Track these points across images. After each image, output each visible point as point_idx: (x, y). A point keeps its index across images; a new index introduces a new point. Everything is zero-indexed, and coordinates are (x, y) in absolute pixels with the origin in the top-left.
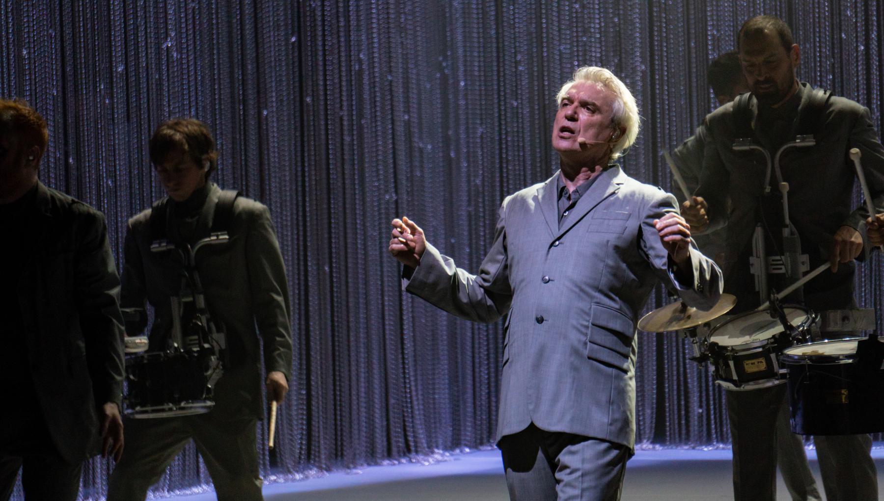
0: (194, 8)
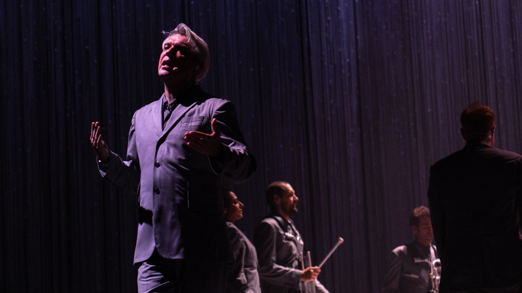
0: (349, 63)
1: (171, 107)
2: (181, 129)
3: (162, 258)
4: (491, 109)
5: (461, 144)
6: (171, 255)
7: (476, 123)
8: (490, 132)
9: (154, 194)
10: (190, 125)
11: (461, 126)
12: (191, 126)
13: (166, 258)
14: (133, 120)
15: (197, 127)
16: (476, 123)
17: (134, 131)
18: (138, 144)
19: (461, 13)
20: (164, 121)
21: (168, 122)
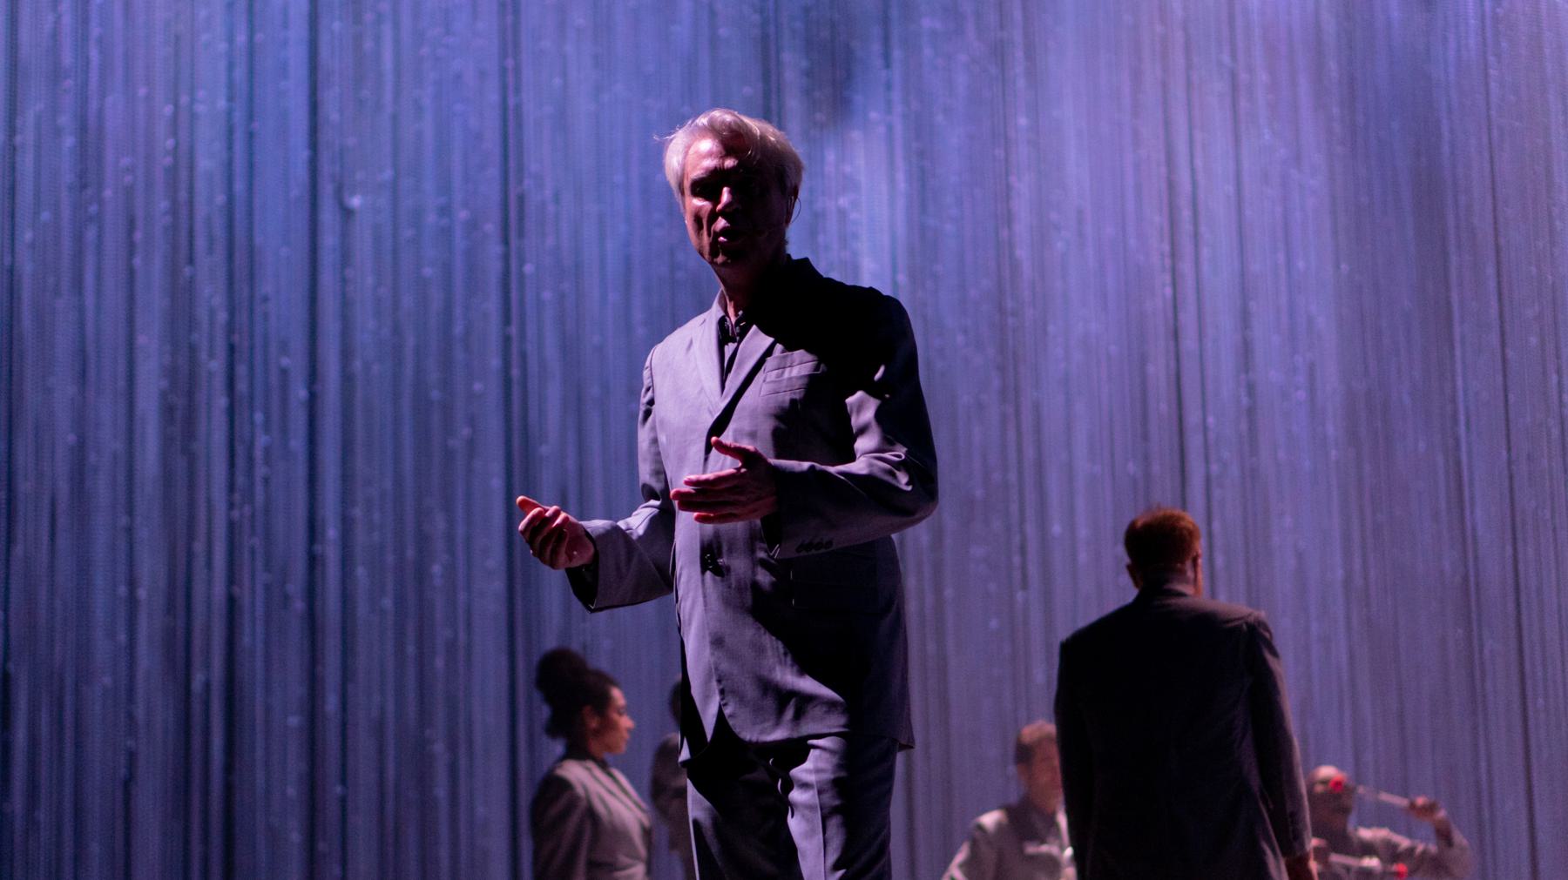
1: (737, 330)
2: (766, 388)
3: (742, 741)
4: (1193, 517)
5: (1124, 592)
6: (762, 732)
7: (1157, 547)
8: (1189, 564)
9: (703, 572)
10: (786, 375)
11: (1127, 560)
12: (790, 379)
13: (750, 742)
14: (646, 373)
15: (805, 381)
16: (1157, 547)
17: (651, 402)
18: (662, 438)
19: (1030, 453)
20: (725, 371)
21: (730, 376)
